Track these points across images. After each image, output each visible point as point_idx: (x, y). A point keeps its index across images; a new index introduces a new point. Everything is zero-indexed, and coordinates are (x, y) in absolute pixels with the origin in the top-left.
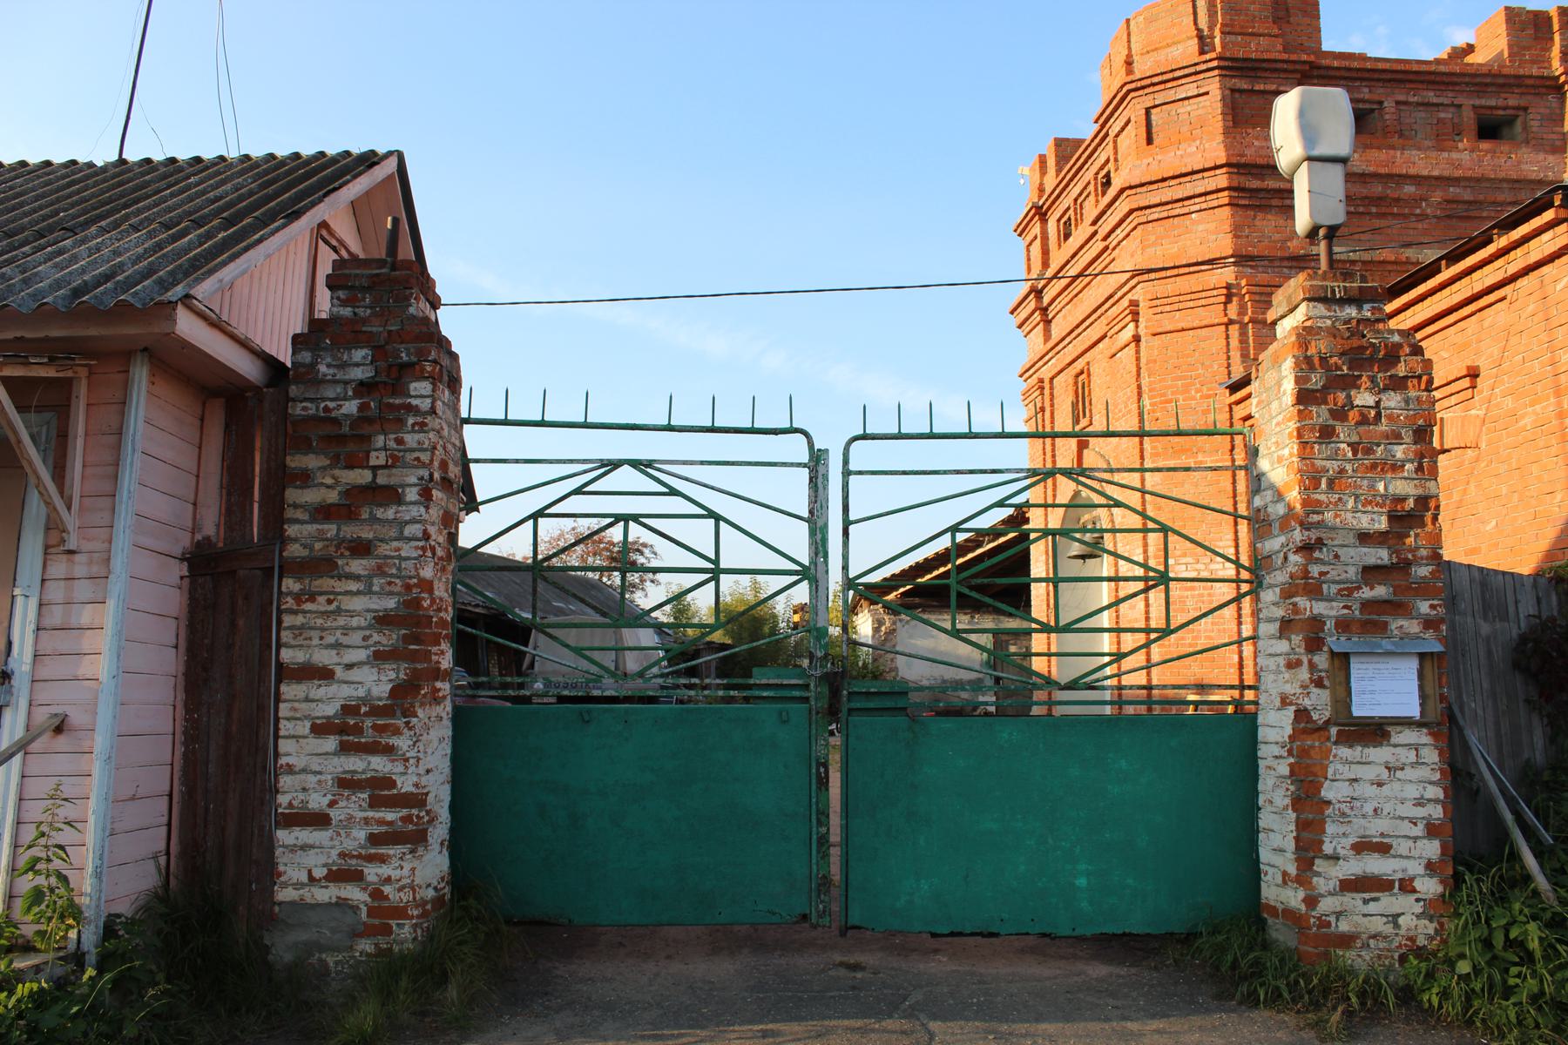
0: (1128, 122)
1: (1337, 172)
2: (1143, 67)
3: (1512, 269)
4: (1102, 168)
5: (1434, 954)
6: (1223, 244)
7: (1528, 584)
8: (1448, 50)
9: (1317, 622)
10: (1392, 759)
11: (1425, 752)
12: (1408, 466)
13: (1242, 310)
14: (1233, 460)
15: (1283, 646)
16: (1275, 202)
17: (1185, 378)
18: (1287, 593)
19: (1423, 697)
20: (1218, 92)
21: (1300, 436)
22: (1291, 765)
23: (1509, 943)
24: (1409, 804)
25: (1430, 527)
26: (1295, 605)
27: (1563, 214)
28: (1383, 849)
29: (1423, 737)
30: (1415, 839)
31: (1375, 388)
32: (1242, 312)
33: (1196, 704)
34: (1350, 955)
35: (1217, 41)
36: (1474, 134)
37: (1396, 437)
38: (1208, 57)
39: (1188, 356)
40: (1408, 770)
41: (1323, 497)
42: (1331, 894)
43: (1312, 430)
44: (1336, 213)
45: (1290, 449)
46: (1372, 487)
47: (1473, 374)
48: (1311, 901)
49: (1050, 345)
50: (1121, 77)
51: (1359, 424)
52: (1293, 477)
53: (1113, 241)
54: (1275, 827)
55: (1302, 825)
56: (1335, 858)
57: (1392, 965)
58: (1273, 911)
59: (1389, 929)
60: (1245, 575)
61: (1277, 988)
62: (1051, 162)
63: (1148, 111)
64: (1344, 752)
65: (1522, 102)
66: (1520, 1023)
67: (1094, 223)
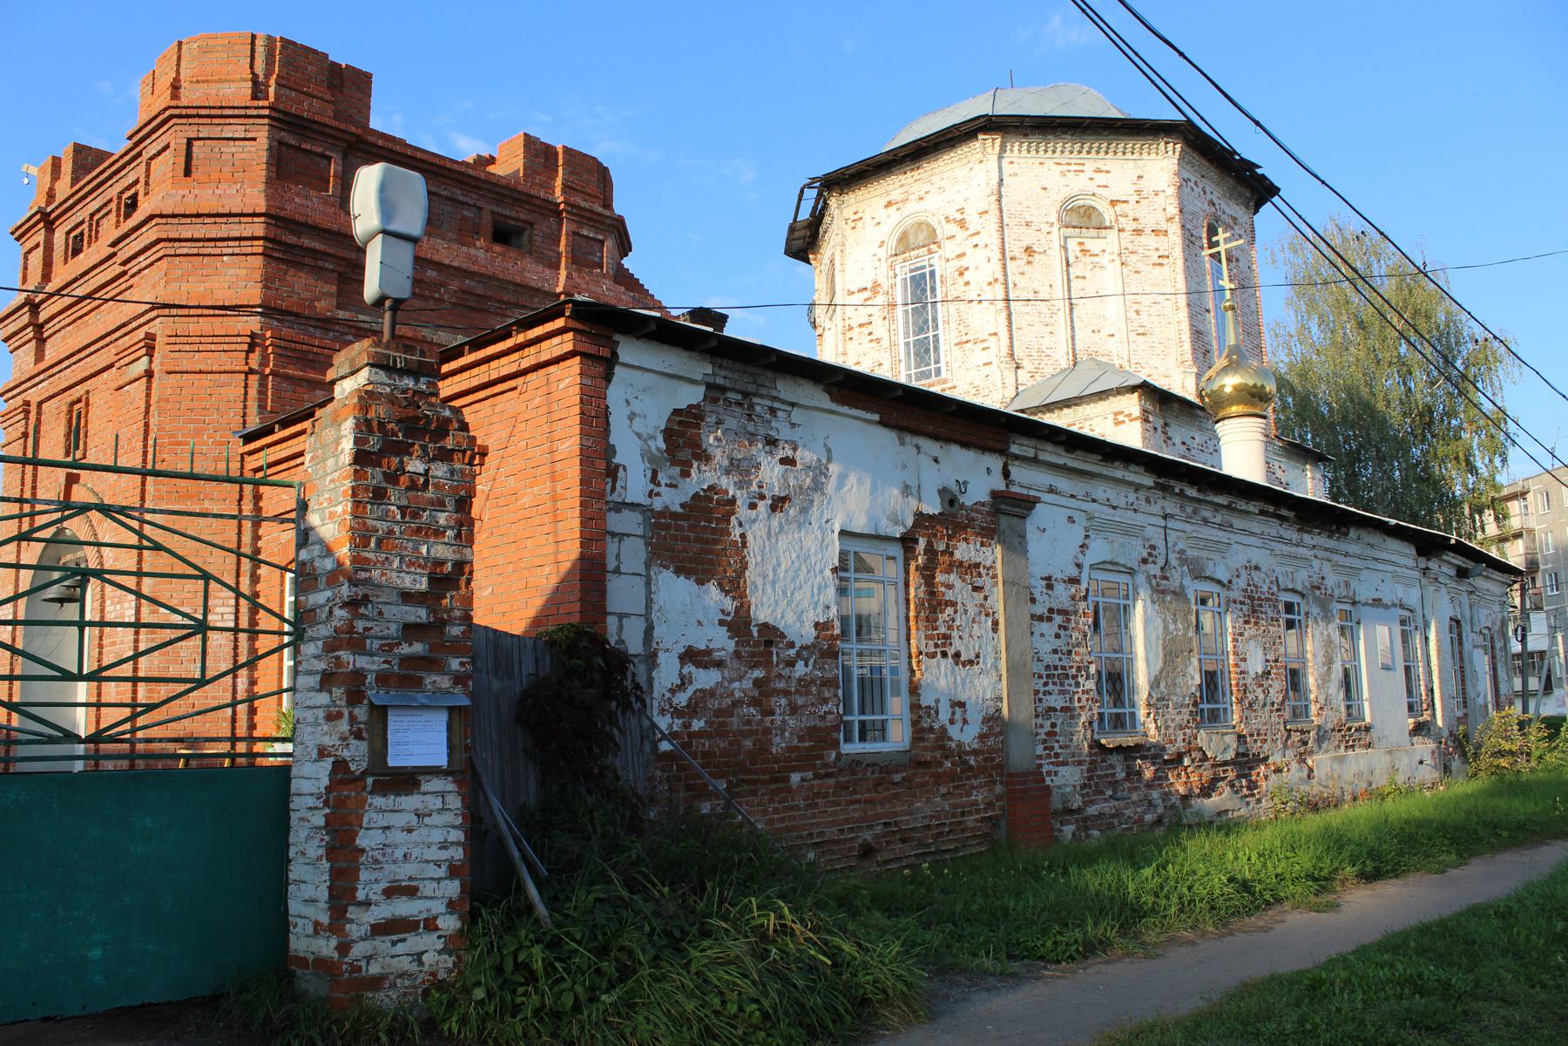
0: (167, 147)
1: (406, 253)
2: (190, 95)
3: (525, 364)
4: (128, 188)
5: (453, 985)
6: (252, 293)
7: (530, 644)
8: (474, 155)
9: (359, 675)
10: (420, 806)
11: (449, 798)
12: (449, 533)
13: (264, 363)
14: (240, 511)
15: (324, 699)
16: (307, 261)
17: (198, 421)
18: (330, 646)
19: (451, 747)
20: (265, 141)
21: (354, 495)
22: (326, 816)
23: (518, 966)
24: (435, 848)
25: (463, 591)
26: (338, 658)
27: (572, 324)
28: (411, 892)
29: (447, 785)
30: (439, 880)
31: (425, 456)
32: (264, 363)
33: (187, 757)
34: (380, 996)
35: (272, 90)
36: (490, 235)
37: (440, 504)
38: (261, 103)
39: (202, 400)
40: (435, 816)
41: (371, 556)
42: (362, 939)
43: (366, 490)
44: (403, 289)
45: (343, 508)
46: (416, 550)
48: (344, 948)
49: (42, 366)
50: (164, 99)
51: (408, 489)
52: (345, 535)
53: (133, 267)
54: (307, 878)
55: (335, 874)
56: (367, 904)
57: (416, 1001)
58: (303, 962)
59: (414, 967)
60: (287, 628)
61: (311, 1038)
62: (67, 168)
63: (190, 142)
64: (379, 801)
65: (530, 218)
66: (525, 1035)
67: (113, 245)
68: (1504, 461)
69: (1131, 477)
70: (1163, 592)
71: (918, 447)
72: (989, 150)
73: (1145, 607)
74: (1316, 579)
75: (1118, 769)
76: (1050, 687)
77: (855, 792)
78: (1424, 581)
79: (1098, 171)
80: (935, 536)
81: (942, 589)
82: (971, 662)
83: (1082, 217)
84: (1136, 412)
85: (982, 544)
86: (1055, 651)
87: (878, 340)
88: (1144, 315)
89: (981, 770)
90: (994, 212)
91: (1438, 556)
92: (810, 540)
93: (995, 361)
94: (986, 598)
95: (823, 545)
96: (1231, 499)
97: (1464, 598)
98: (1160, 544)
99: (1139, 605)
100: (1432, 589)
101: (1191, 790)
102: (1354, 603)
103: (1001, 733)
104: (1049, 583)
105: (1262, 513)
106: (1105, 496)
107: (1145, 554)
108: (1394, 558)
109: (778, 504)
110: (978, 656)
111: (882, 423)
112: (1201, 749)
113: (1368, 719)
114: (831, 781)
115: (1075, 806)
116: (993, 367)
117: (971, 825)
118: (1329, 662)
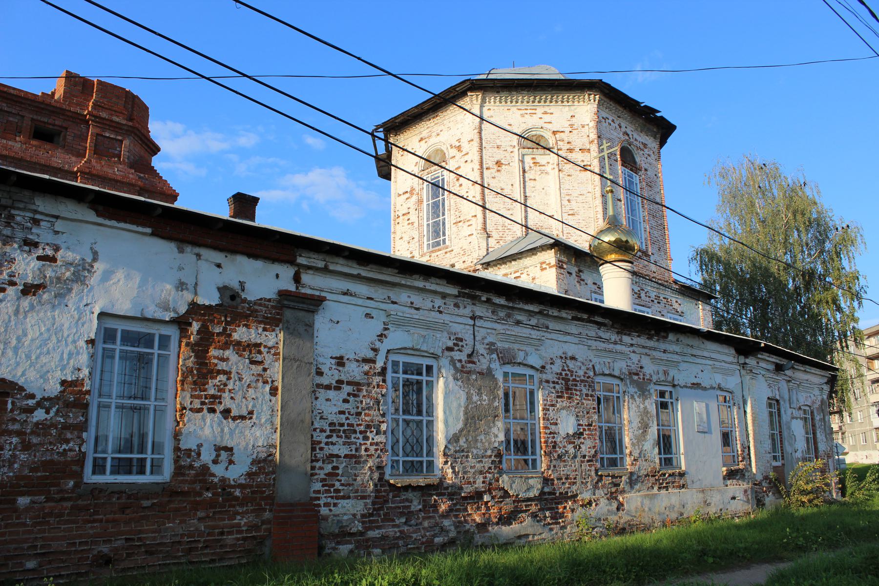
47: (338, 322)
68: (860, 303)
69: (433, 287)
70: (469, 372)
71: (198, 256)
72: (475, 102)
73: (446, 385)
74: (634, 368)
75: (415, 503)
76: (334, 439)
77: (96, 513)
78: (743, 372)
79: (545, 113)
80: (212, 321)
81: (216, 361)
82: (243, 418)
83: (533, 142)
84: (553, 261)
85: (265, 330)
86: (342, 412)
87: (412, 223)
88: (573, 203)
89: (243, 501)
90: (477, 139)
91: (755, 355)
92: (65, 318)
93: (475, 233)
94: (265, 370)
95: (79, 322)
96: (542, 307)
97: (784, 385)
98: (468, 338)
99: (441, 381)
100: (748, 377)
101: (489, 519)
102: (674, 386)
103: (273, 472)
104: (340, 362)
105: (575, 318)
106: (409, 300)
107: (450, 344)
108: (714, 356)
109: (29, 290)
110: (251, 413)
111: (153, 234)
112: (503, 489)
113: (683, 468)
114: (68, 504)
115: (354, 530)
116: (473, 237)
117: (229, 542)
118: (645, 427)
